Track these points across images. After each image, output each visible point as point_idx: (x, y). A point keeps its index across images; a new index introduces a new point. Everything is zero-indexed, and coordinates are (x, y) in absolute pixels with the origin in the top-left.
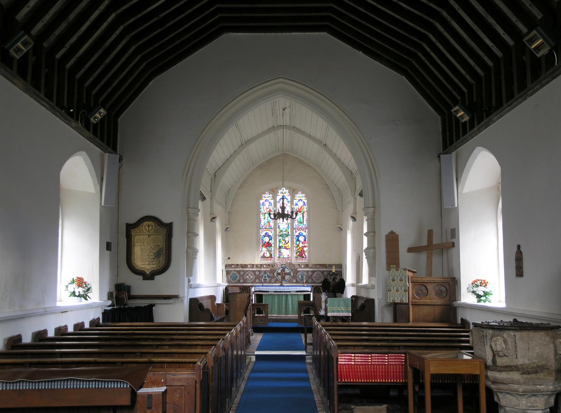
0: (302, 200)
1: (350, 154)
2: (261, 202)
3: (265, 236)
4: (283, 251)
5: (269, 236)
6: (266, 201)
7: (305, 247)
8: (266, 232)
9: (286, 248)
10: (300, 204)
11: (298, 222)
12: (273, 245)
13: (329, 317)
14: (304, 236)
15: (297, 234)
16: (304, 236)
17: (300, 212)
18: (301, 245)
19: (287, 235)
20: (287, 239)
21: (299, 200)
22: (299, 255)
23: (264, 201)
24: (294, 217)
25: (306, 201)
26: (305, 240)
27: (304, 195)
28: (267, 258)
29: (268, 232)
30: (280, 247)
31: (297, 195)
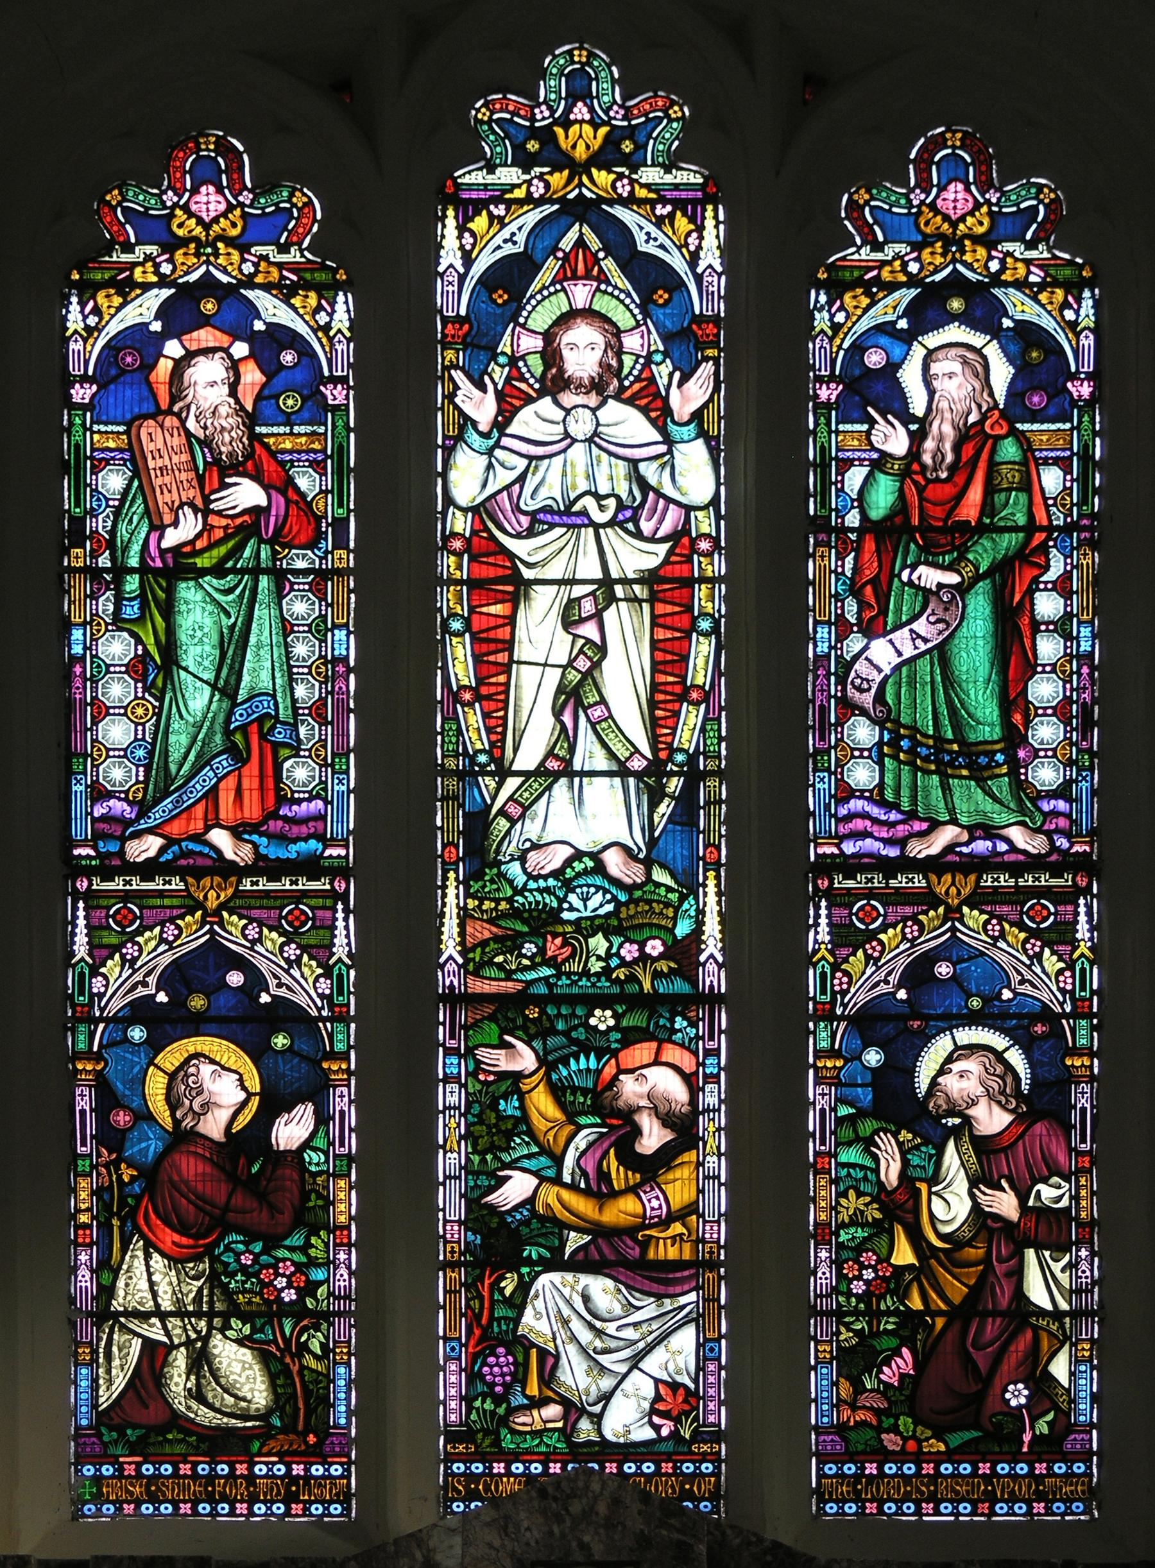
0: (983, 312)
1: (996, 713)
2: (93, 326)
3: (165, 1023)
4: (556, 1305)
5: (252, 1022)
6: (181, 313)
7: (1048, 1230)
8: (191, 935)
9: (619, 1255)
10: (950, 378)
11: (898, 741)
12: (346, 1203)
13: (887, 518)
14: (1031, 1026)
15: (869, 980)
16: (1031, 1026)
17: (946, 539)
18: (951, 1206)
19: (650, 1014)
20: (653, 1083)
21: (927, 311)
22: (906, 1397)
23: (144, 309)
24: (320, 334)
25: (1076, 324)
26: (1040, 1104)
27: (1032, 194)
28: (218, 1442)
29: (235, 932)
30: (507, 1246)
31: (890, 199)
